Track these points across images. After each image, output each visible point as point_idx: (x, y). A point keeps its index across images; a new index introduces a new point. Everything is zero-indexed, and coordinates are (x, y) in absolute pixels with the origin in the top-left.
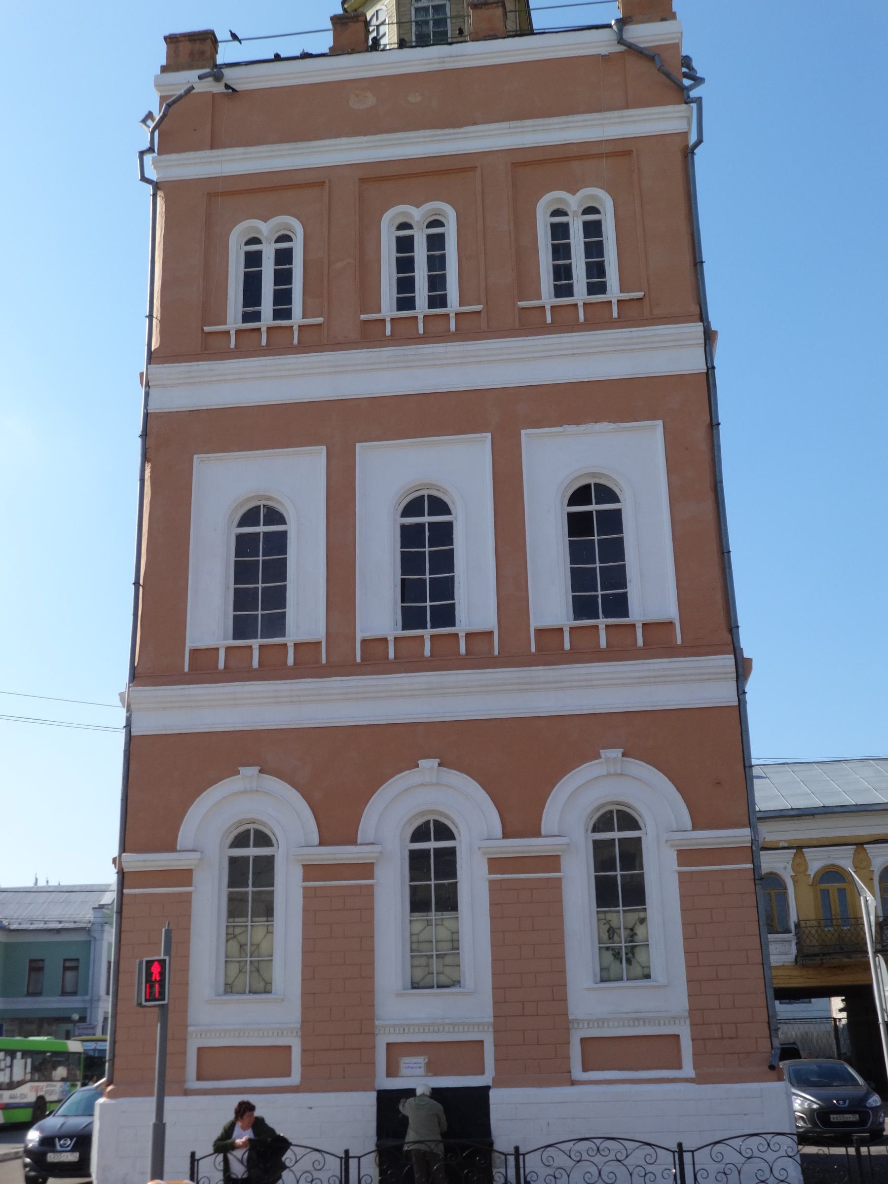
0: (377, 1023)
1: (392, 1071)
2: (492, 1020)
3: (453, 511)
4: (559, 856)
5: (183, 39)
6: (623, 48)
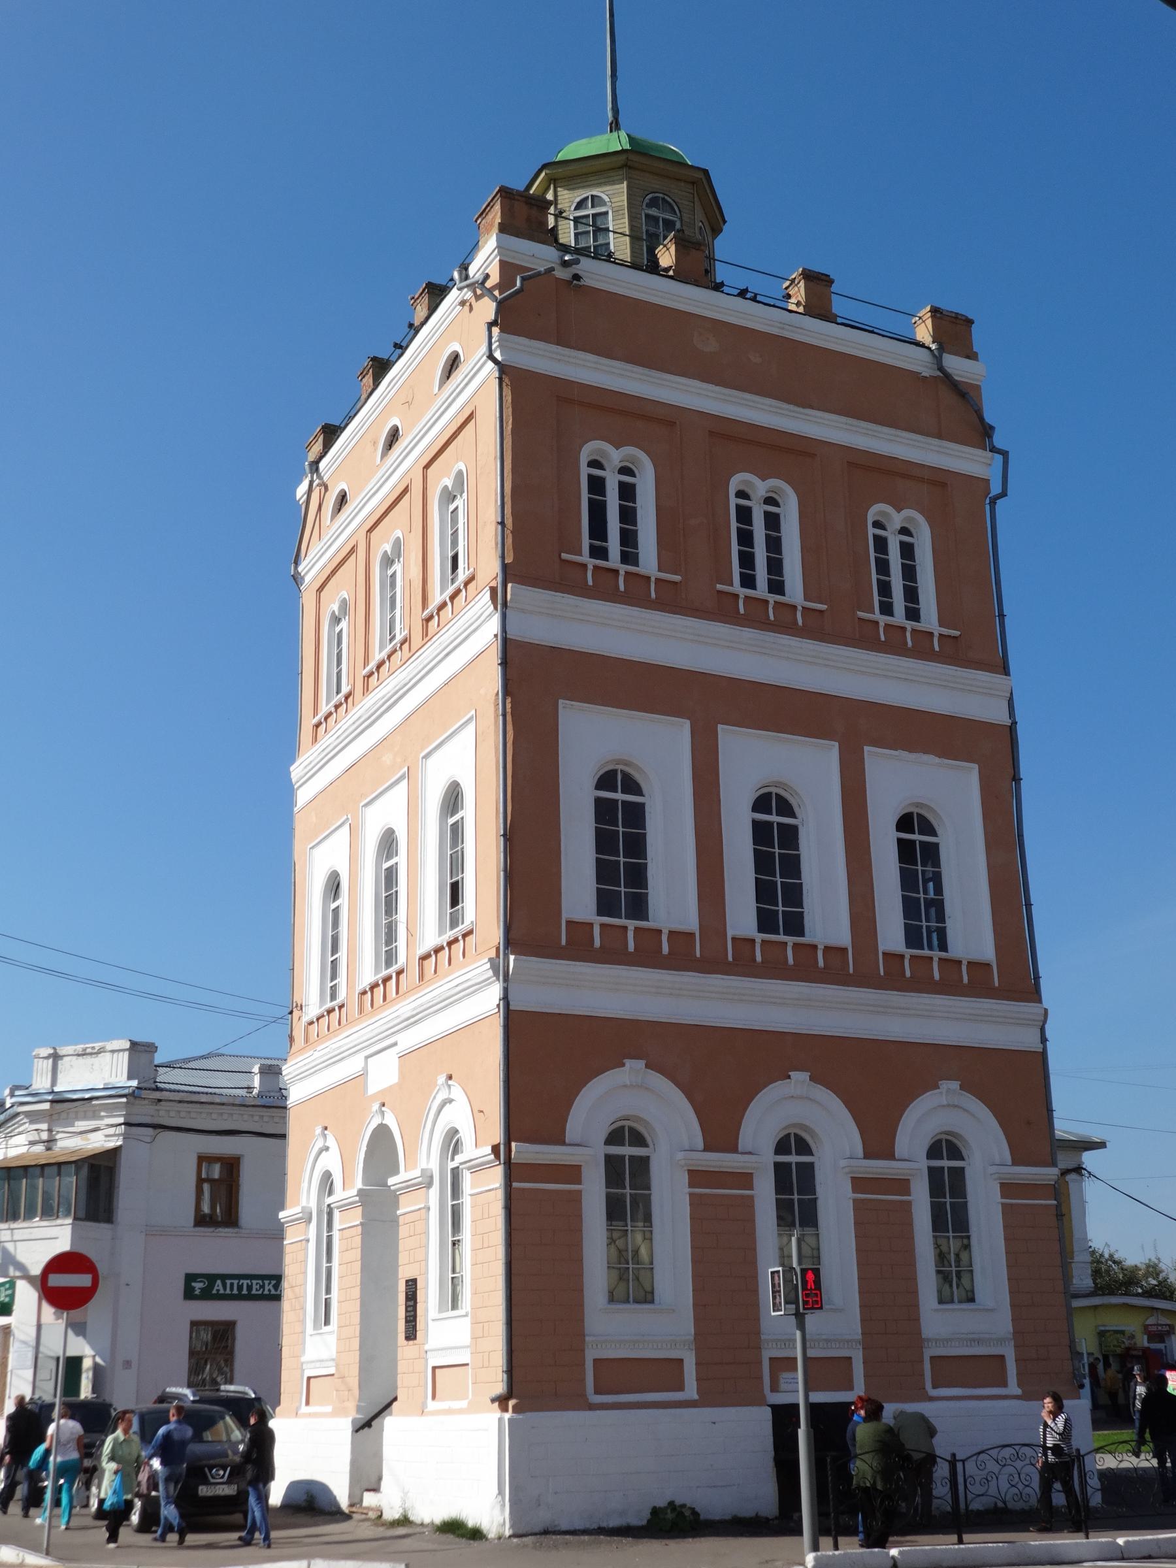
0: (763, 1337)
1: (775, 1388)
2: (860, 1337)
3: (797, 814)
4: (752, 1174)
5: (519, 198)
6: (939, 373)
